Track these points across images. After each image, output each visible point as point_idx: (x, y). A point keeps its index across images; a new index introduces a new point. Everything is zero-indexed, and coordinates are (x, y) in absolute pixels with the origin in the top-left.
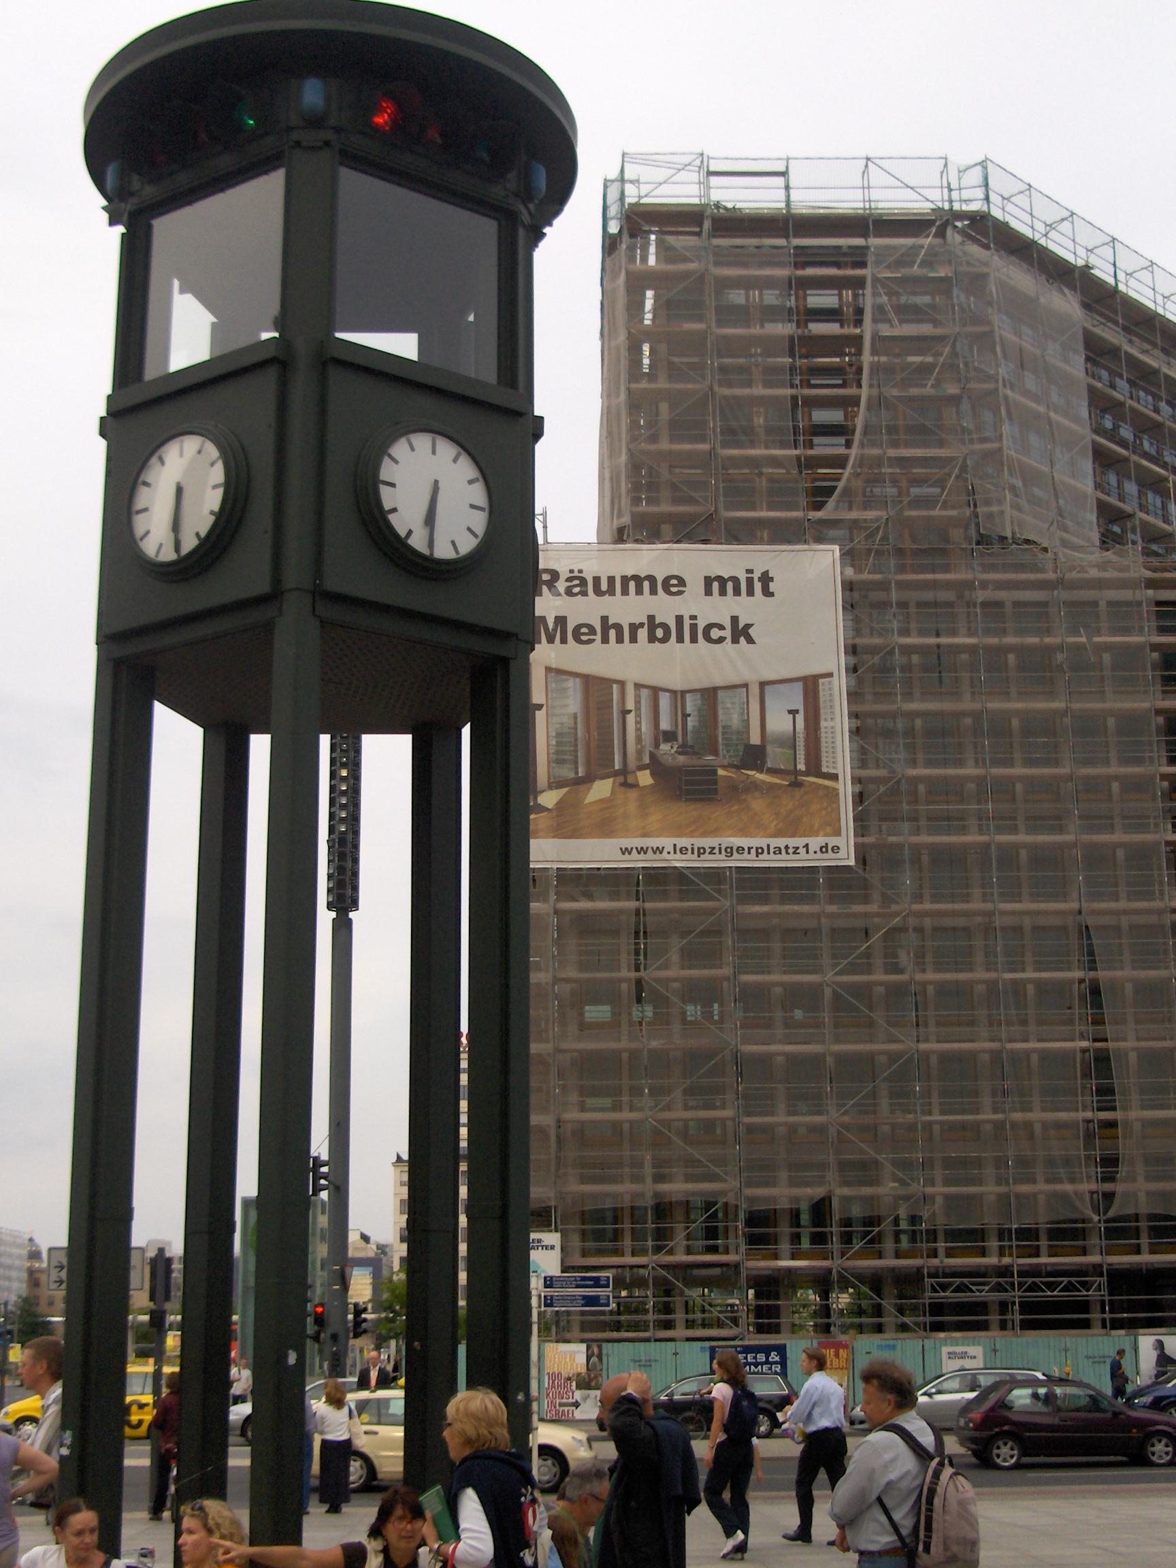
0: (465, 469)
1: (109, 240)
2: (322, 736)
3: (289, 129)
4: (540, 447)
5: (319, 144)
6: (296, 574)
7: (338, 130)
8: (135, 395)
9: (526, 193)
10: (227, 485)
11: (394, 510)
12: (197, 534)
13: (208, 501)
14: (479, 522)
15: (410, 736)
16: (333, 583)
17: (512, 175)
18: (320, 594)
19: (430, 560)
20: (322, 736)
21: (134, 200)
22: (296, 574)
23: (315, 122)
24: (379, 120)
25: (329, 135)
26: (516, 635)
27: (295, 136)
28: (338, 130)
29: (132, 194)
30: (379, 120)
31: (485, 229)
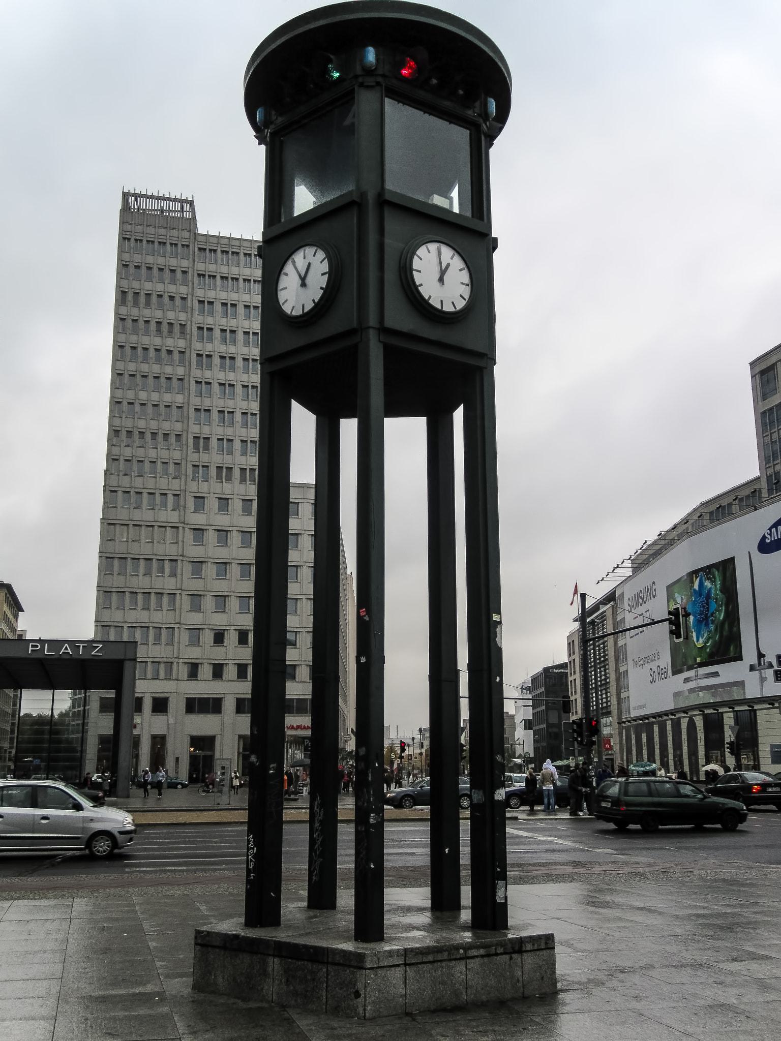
0: (425, 292)
1: (256, 155)
2: (343, 422)
3: (356, 77)
4: (496, 255)
5: (374, 84)
6: (373, 321)
7: (383, 76)
8: (277, 230)
9: (485, 115)
10: (330, 273)
11: (421, 285)
12: (314, 301)
13: (319, 280)
14: (466, 292)
15: (423, 421)
16: (389, 323)
17: (477, 104)
18: (384, 330)
19: (441, 311)
20: (343, 422)
21: (272, 126)
22: (373, 321)
23: (369, 72)
24: (405, 72)
25: (380, 79)
26: (486, 355)
27: (360, 80)
28: (383, 76)
29: (272, 123)
30: (405, 72)
31: (461, 135)
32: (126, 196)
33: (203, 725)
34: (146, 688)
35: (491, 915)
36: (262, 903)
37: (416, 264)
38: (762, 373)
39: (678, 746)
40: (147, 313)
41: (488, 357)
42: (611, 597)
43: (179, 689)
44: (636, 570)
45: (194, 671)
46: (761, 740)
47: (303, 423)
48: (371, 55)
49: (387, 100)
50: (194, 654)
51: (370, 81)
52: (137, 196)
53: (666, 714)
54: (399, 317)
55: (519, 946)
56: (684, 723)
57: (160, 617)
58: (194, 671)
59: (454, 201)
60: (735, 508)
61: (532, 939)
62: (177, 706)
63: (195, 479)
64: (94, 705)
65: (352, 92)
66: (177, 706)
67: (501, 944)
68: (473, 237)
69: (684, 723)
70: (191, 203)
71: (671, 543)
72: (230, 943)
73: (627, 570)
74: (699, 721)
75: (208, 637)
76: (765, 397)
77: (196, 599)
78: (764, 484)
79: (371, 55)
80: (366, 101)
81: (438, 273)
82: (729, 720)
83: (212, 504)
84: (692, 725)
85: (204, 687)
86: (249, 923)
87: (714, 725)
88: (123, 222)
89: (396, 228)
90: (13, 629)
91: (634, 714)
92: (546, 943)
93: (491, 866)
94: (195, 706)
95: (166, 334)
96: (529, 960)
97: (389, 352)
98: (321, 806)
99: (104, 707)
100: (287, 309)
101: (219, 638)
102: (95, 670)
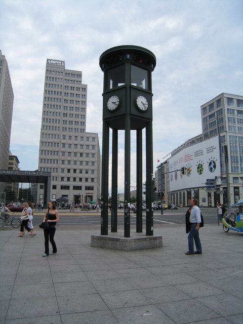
6: (129, 113)
8: (107, 91)
16: (132, 113)
18: (130, 114)
31: (146, 72)
32: (48, 60)
33: (77, 192)
34: (53, 183)
35: (150, 232)
36: (104, 231)
37: (137, 100)
38: (204, 109)
39: (180, 198)
40: (52, 89)
41: (151, 119)
42: (166, 162)
43: (59, 183)
44: (172, 156)
45: (62, 179)
46: (200, 197)
47: (111, 130)
48: (128, 56)
49: (132, 66)
50: (62, 175)
51: (128, 61)
52: (50, 60)
53: (178, 191)
54: (134, 112)
55: (155, 238)
56: (182, 193)
57: (54, 166)
58: (62, 179)
59: (144, 85)
60: (196, 141)
61: (158, 237)
62: (58, 187)
63: (63, 131)
64: (39, 187)
65: (124, 63)
66: (58, 187)
67: (153, 238)
68: (148, 94)
69: (182, 193)
70: (64, 62)
71: (181, 150)
72: (99, 238)
73: (170, 156)
74: (186, 192)
75: (66, 171)
76: (204, 115)
77: (63, 162)
78: (203, 136)
79: (128, 56)
80: (127, 65)
81: (141, 101)
82: (193, 192)
83: (67, 137)
84: (184, 194)
85: (65, 183)
86: (101, 234)
87: (189, 193)
88: (47, 67)
89: (133, 92)
90: (17, 167)
91: (171, 190)
92: (161, 238)
93: (150, 223)
94: (75, 188)
95: (59, 94)
96: (158, 241)
97: (131, 119)
98: (114, 212)
99: (41, 187)
100: (109, 108)
101: (69, 171)
102: (40, 179)
